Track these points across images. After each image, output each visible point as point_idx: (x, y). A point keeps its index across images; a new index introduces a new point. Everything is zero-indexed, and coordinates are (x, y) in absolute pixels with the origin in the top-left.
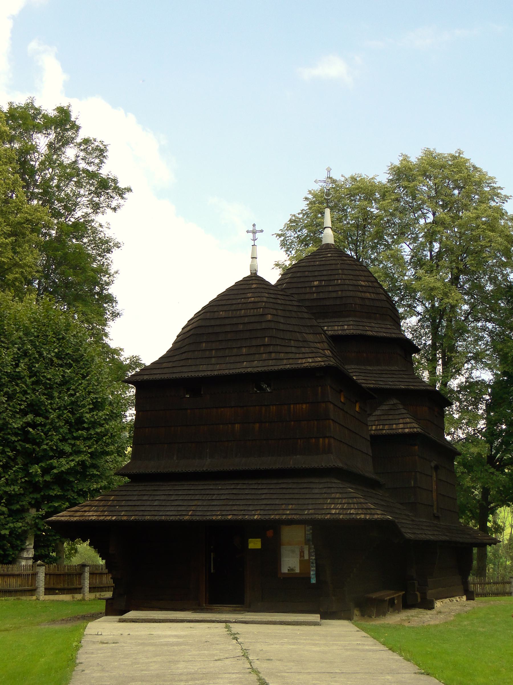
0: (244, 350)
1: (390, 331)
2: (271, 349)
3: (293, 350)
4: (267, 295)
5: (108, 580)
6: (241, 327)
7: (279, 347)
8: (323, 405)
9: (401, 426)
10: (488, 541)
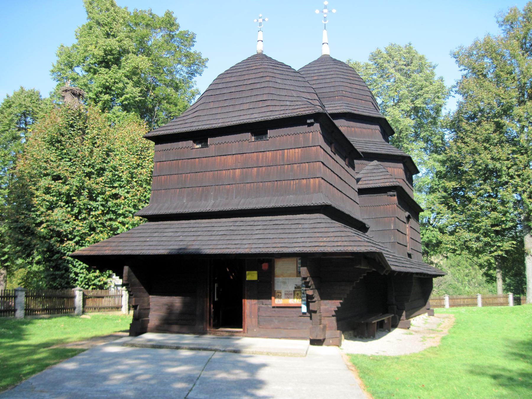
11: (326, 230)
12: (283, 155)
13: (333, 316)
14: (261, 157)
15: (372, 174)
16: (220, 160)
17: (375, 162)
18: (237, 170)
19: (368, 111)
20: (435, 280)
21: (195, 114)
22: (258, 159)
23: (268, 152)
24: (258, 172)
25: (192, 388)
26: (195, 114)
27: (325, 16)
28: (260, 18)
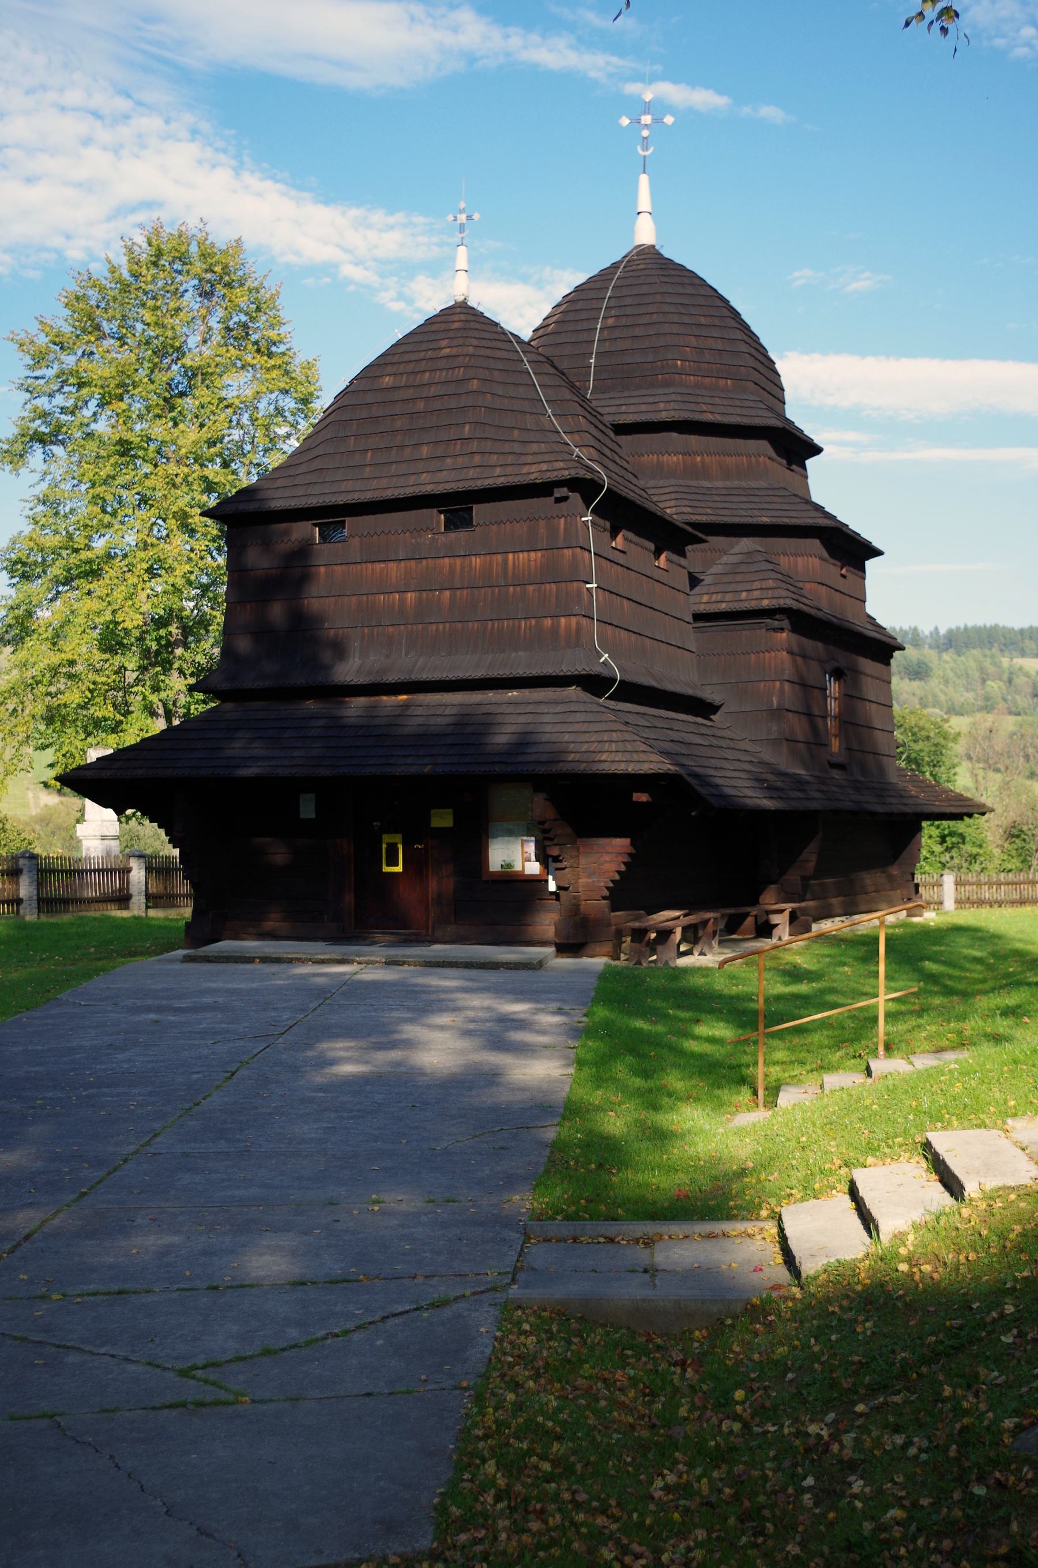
0: (425, 451)
1: (752, 412)
2: (474, 446)
3: (517, 448)
4: (475, 342)
5: (183, 886)
6: (421, 406)
7: (489, 443)
8: (568, 552)
9: (757, 594)
10: (965, 810)
11: (584, 727)
12: (505, 561)
13: (604, 898)
14: (458, 568)
15: (732, 575)
16: (373, 570)
17: (746, 544)
18: (409, 595)
19: (738, 411)
20: (929, 832)
21: (317, 464)
22: (452, 570)
23: (473, 558)
24: (453, 598)
25: (261, 1355)
26: (317, 464)
27: (645, 133)
28: (461, 211)
